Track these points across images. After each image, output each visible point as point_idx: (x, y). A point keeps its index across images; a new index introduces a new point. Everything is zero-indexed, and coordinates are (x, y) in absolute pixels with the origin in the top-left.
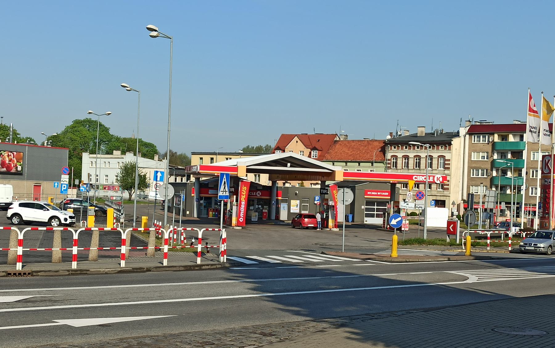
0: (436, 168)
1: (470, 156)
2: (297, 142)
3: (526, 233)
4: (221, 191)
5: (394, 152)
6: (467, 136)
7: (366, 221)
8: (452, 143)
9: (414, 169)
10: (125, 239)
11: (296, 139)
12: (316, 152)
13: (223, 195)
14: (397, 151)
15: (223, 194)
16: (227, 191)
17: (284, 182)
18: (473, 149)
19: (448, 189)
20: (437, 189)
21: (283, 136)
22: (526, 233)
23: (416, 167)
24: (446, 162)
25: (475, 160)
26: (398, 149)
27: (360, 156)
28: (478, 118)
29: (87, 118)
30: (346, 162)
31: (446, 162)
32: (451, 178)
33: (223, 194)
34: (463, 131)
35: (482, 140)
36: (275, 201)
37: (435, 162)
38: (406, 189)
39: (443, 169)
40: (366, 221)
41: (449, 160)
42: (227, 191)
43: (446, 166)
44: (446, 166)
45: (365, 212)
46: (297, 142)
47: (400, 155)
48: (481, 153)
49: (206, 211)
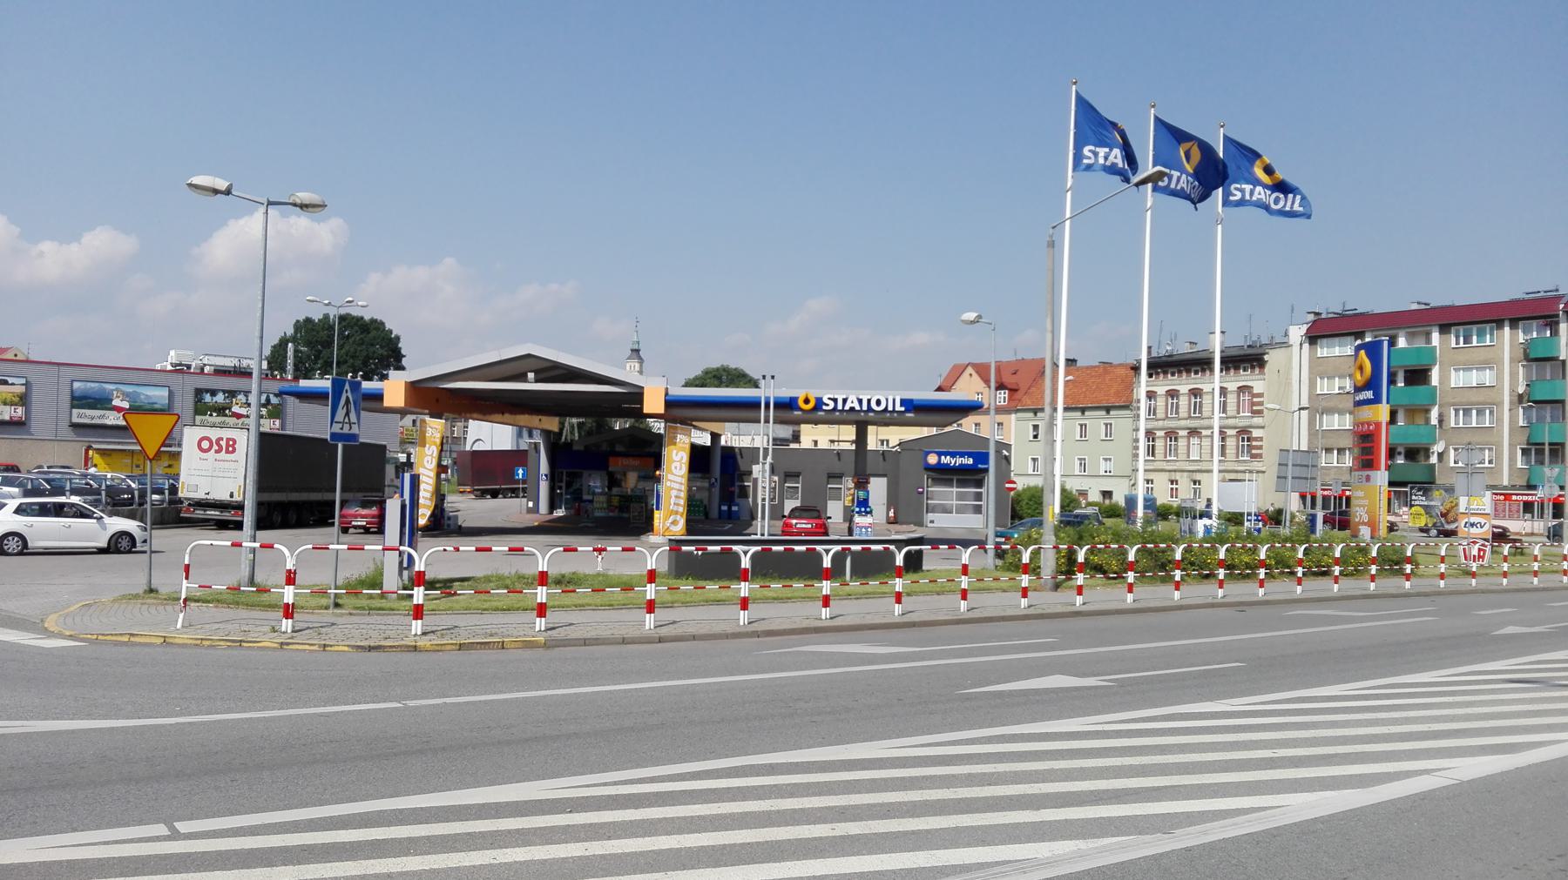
0: (1234, 413)
1: (1312, 385)
2: (971, 375)
3: (1304, 546)
4: (336, 420)
5: (1173, 382)
6: (1306, 346)
7: (932, 522)
8: (1266, 357)
9: (1167, 417)
10: (424, 572)
11: (970, 370)
12: (1005, 393)
13: (341, 431)
14: (1155, 383)
15: (342, 429)
16: (354, 423)
17: (793, 446)
18: (1319, 369)
19: (1260, 456)
20: (1166, 457)
21: (955, 367)
22: (1304, 546)
23: (1195, 413)
24: (1255, 400)
25: (1326, 392)
26: (1180, 376)
27: (1085, 397)
28: (1331, 306)
29: (398, 338)
30: (1083, 410)
31: (1255, 400)
32: (1401, 445)
33: (342, 429)
34: (1297, 333)
35: (1342, 349)
36: (716, 479)
37: (1232, 401)
38: (1153, 458)
39: (1250, 414)
40: (932, 522)
41: (1260, 395)
42: (354, 423)
43: (1255, 408)
44: (1255, 408)
45: (799, 485)
46: (971, 375)
47: (1184, 389)
48: (1337, 379)
49: (9, 397)
